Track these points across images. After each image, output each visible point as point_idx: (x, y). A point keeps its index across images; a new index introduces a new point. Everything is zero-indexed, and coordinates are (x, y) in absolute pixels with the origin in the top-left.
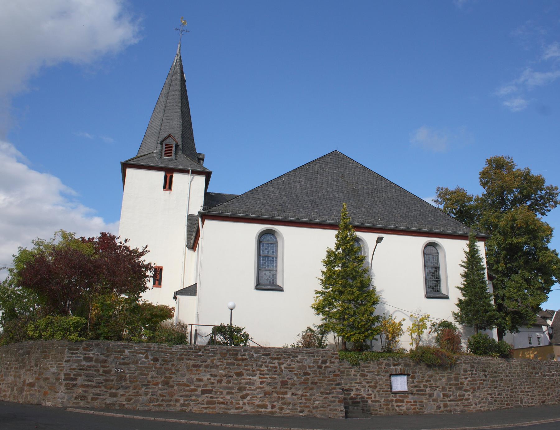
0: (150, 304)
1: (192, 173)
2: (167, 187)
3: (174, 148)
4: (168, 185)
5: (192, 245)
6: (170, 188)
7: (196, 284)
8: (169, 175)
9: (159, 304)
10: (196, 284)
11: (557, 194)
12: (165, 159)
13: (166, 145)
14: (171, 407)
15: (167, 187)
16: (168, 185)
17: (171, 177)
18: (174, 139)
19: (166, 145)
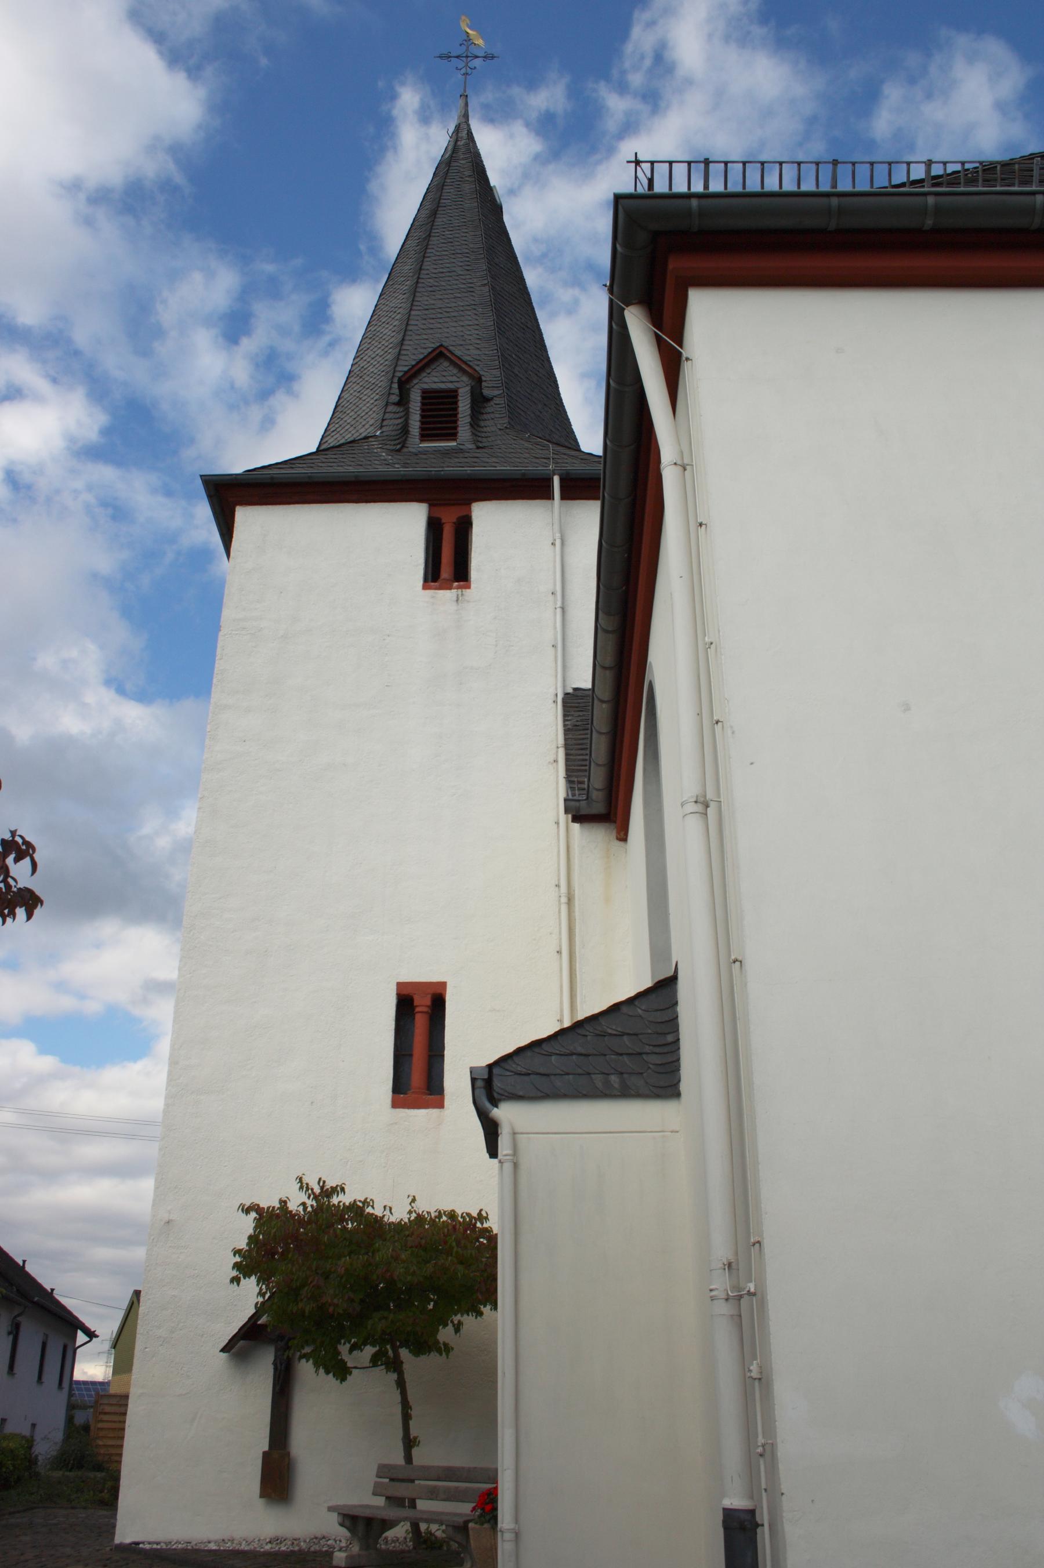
0: (357, 1210)
1: (563, 497)
2: (446, 571)
3: (464, 406)
4: (448, 562)
5: (597, 796)
6: (461, 575)
7: (665, 988)
8: (449, 518)
9: (428, 1206)
10: (665, 988)
11: (468, 1214)
12: (425, 452)
13: (428, 396)
14: (694, 825)
15: (446, 571)
16: (448, 562)
17: (464, 528)
18: (459, 365)
19: (428, 396)
